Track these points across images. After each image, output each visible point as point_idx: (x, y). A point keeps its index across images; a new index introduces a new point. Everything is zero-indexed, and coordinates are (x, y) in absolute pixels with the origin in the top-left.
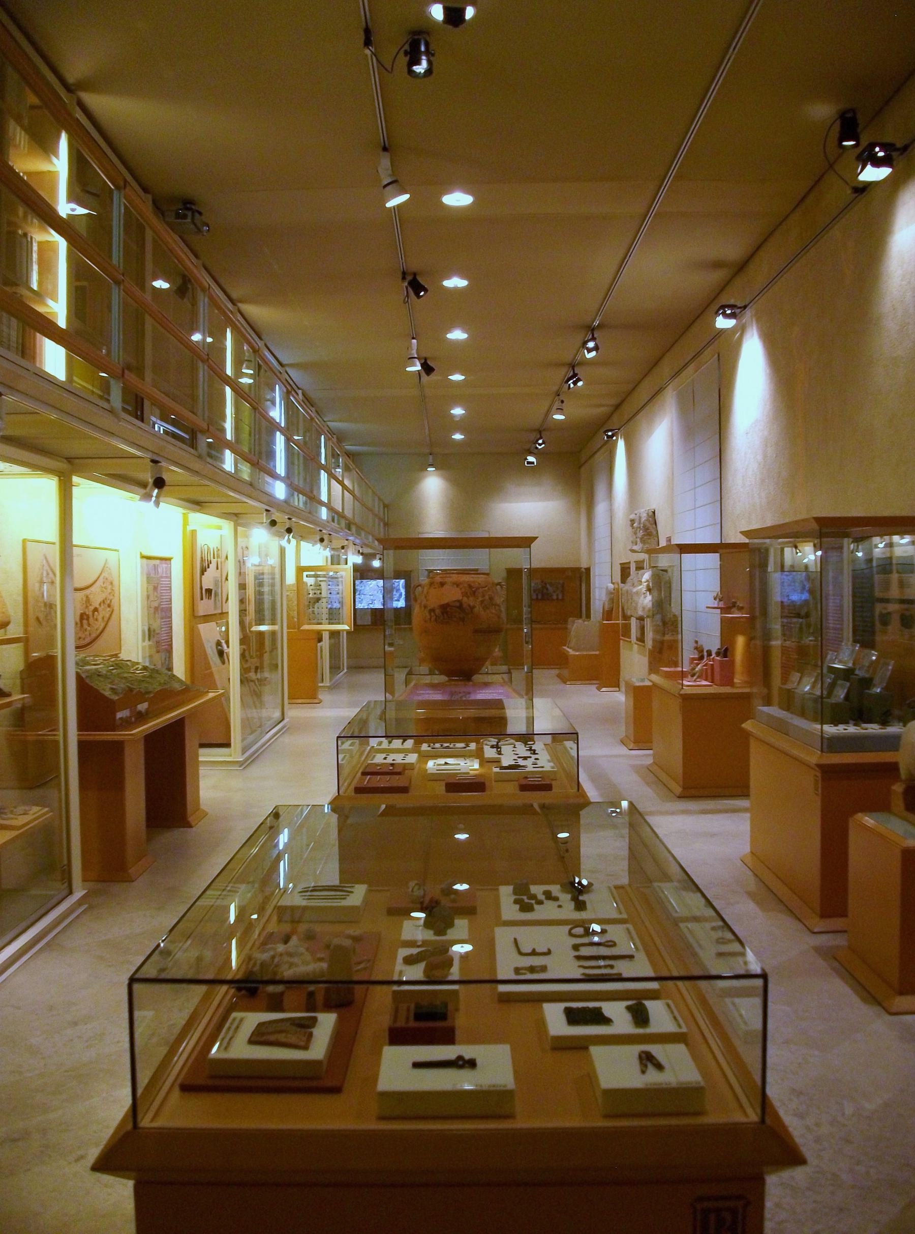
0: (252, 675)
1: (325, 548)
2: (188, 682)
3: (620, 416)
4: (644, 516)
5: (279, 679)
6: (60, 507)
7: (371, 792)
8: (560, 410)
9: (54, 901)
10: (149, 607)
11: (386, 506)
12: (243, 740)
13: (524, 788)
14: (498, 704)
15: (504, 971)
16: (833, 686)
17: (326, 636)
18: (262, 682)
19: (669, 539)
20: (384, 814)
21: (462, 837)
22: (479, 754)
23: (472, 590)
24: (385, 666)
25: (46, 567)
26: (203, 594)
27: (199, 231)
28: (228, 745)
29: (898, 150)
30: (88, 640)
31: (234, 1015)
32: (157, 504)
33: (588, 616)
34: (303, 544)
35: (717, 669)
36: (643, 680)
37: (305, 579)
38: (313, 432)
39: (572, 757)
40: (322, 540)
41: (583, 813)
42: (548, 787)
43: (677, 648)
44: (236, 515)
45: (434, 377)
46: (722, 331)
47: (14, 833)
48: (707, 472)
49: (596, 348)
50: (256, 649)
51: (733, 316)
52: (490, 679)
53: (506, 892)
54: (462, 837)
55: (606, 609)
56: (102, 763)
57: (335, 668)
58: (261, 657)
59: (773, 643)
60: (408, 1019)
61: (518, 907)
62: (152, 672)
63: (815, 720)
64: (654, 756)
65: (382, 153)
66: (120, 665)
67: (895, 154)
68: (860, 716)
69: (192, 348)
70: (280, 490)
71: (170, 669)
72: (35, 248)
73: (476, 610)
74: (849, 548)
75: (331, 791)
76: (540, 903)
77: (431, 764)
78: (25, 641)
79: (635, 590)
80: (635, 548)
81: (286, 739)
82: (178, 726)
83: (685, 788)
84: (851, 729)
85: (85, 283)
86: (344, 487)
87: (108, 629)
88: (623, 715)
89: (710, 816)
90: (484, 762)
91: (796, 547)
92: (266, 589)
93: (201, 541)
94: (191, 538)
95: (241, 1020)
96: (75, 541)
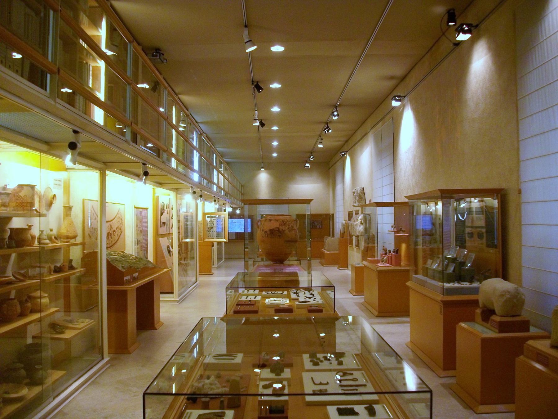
0: (183, 262)
1: (216, 204)
2: (155, 263)
3: (348, 145)
4: (359, 191)
5: (196, 263)
6: (101, 183)
7: (241, 313)
8: (321, 143)
9: (95, 363)
10: (137, 230)
11: (242, 186)
12: (179, 291)
13: (310, 311)
14: (296, 274)
15: (308, 390)
16: (447, 265)
17: (215, 244)
18: (187, 265)
19: (370, 201)
20: (244, 324)
21: (276, 335)
22: (288, 296)
23: (284, 223)
24: (246, 257)
25: (93, 212)
26: (161, 225)
27: (163, 62)
28: (172, 293)
29: (473, 27)
30: (111, 245)
31: (188, 411)
32: (145, 183)
33: (333, 236)
34: (205, 202)
35: (393, 258)
36: (359, 264)
37: (207, 218)
38: (211, 152)
39: (331, 298)
40: (215, 201)
41: (337, 323)
42: (321, 311)
43: (374, 251)
44: (177, 189)
45: (265, 128)
46: (394, 107)
47: (77, 332)
48: (388, 170)
49: (338, 115)
50: (185, 249)
51: (399, 100)
52: (291, 263)
53: (306, 357)
54: (276, 335)
55: (342, 232)
56: (117, 300)
57: (219, 259)
58: (187, 253)
59: (419, 247)
60: (266, 414)
61: (312, 363)
62: (139, 259)
63: (439, 281)
64: (365, 298)
65: (245, 28)
66: (126, 256)
67: (472, 29)
68: (460, 279)
69: (160, 113)
70: (196, 177)
71: (147, 258)
72: (91, 69)
73: (286, 232)
74: (453, 205)
75: (222, 313)
76: (322, 361)
77: (267, 301)
78: (83, 244)
79: (355, 223)
80: (355, 204)
81: (198, 291)
82: (151, 283)
83: (379, 312)
84: (456, 285)
85: (113, 85)
86: (224, 177)
87: (120, 239)
88: (350, 280)
89: (391, 325)
90: (291, 300)
91: (427, 204)
92: (189, 223)
93: (161, 201)
94: (156, 200)
95: (191, 413)
96: (107, 201)
